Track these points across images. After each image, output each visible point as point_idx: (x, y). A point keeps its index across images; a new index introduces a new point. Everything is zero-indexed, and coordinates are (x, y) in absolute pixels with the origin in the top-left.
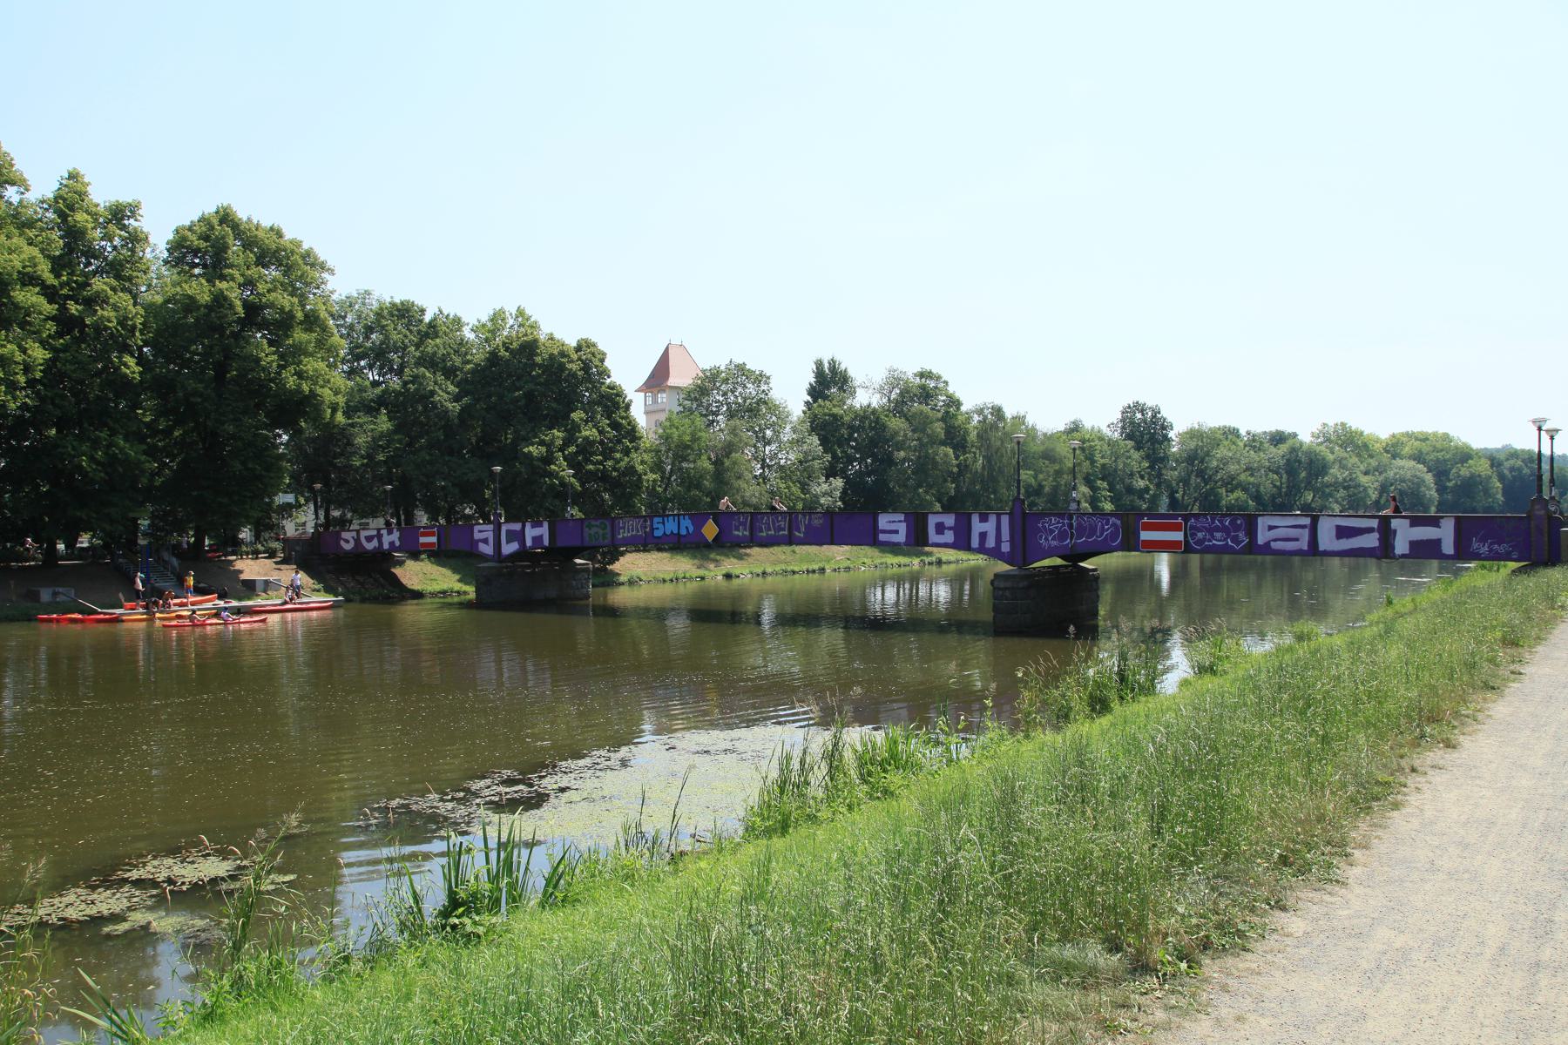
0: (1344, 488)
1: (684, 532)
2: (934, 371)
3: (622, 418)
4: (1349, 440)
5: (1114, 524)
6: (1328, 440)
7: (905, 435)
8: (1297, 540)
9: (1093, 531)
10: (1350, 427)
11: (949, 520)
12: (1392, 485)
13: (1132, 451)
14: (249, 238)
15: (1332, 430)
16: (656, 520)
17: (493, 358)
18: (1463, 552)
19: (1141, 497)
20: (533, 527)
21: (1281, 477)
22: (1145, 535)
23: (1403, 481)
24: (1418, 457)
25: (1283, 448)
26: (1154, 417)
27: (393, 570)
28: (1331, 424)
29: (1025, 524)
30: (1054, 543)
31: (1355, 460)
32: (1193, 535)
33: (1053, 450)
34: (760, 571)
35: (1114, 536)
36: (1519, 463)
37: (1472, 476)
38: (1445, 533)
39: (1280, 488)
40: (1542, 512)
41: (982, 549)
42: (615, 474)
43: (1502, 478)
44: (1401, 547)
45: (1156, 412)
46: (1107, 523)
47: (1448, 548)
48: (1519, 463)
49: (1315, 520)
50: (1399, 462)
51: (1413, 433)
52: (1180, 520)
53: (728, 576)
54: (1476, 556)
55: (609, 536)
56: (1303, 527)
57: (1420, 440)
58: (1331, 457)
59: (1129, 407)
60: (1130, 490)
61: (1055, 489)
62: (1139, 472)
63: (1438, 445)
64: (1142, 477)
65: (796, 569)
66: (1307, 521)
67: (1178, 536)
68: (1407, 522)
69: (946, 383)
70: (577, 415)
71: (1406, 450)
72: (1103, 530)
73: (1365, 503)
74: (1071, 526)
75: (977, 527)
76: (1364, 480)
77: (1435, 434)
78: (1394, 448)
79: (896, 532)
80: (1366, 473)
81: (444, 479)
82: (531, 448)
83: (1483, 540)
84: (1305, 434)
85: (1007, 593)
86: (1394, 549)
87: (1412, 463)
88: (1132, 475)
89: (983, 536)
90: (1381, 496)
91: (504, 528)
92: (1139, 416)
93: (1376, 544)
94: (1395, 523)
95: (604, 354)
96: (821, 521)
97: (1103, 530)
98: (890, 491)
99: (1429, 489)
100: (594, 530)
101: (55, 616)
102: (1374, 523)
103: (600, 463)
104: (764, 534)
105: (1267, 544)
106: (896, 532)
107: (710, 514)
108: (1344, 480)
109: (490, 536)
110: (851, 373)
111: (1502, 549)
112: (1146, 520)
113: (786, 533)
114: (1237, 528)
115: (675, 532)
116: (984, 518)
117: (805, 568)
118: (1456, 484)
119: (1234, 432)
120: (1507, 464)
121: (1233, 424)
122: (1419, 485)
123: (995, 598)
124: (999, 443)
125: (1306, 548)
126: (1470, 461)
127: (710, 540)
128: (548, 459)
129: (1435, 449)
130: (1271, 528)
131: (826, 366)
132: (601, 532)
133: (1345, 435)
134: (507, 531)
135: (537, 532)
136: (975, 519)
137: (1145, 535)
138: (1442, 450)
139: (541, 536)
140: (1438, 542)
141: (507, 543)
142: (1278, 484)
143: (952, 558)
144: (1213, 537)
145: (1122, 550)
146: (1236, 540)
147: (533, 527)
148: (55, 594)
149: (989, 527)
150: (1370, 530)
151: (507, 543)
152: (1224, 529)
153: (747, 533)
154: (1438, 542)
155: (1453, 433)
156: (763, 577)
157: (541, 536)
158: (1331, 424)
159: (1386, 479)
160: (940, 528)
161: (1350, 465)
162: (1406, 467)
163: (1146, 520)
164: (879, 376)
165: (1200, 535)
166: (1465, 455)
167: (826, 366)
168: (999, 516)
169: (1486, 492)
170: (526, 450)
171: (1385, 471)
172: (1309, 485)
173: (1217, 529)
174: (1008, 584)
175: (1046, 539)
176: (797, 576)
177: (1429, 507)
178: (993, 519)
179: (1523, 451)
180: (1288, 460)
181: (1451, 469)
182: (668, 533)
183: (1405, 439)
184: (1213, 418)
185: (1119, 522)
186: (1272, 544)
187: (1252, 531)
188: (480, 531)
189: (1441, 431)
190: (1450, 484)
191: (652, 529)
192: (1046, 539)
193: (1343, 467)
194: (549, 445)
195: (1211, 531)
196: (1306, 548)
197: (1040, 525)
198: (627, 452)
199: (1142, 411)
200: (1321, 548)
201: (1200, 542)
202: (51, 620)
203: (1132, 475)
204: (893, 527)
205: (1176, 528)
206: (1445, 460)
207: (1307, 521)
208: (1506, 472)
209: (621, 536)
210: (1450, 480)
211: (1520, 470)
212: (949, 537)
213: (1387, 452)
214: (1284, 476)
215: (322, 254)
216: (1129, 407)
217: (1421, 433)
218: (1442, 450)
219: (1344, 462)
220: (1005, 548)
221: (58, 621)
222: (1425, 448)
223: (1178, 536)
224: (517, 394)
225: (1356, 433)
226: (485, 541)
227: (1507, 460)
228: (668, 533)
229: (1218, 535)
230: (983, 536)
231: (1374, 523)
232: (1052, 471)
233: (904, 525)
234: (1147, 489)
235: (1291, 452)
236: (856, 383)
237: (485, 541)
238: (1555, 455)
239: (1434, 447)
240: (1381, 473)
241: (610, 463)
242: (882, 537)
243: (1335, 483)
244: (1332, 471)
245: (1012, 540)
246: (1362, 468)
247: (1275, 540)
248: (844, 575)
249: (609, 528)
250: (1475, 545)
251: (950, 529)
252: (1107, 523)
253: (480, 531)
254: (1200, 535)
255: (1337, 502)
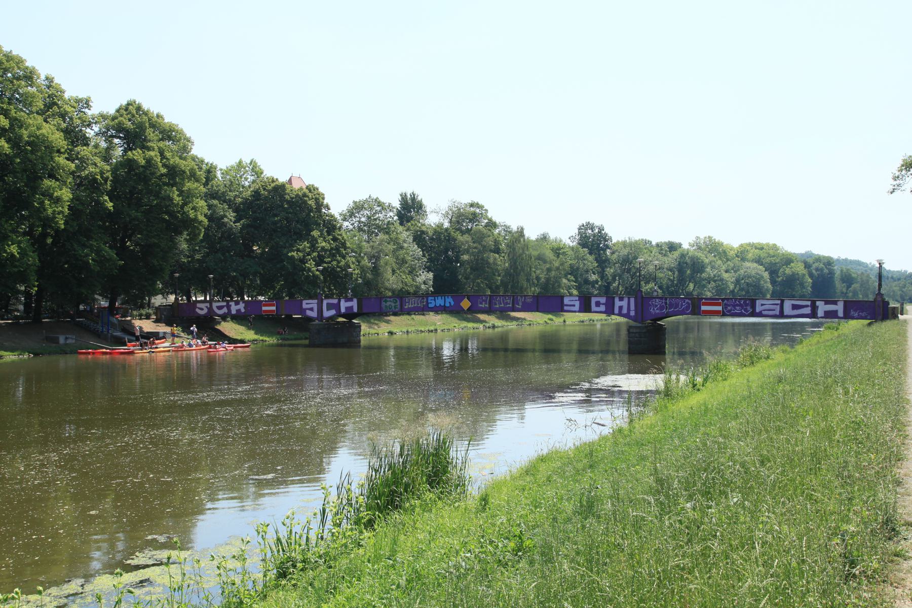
0: (715, 281)
1: (447, 305)
2: (480, 203)
3: (338, 235)
4: (714, 248)
5: (688, 303)
6: (699, 248)
7: (469, 246)
8: (774, 310)
9: (677, 306)
10: (715, 239)
11: (603, 300)
12: (742, 279)
13: (588, 255)
14: (155, 123)
15: (702, 242)
16: (430, 298)
17: (256, 193)
18: (847, 316)
19: (593, 287)
20: (346, 301)
21: (674, 274)
22: (704, 308)
23: (749, 277)
24: (759, 261)
25: (676, 254)
26: (599, 232)
27: (216, 327)
28: (702, 237)
29: (643, 301)
30: (658, 311)
31: (719, 262)
32: (726, 308)
33: (544, 254)
34: (405, 330)
35: (687, 308)
36: (822, 265)
37: (793, 274)
38: (840, 308)
39: (672, 281)
40: (880, 299)
41: (620, 314)
42: (339, 269)
43: (811, 275)
44: (820, 313)
45: (601, 229)
46: (684, 302)
47: (841, 314)
48: (822, 265)
49: (782, 301)
50: (747, 264)
51: (753, 244)
52: (720, 301)
53: (391, 333)
54: (853, 318)
55: (399, 307)
56: (567, 305)
57: (759, 249)
58: (707, 261)
59: (583, 226)
60: (587, 281)
61: (548, 280)
62: (592, 270)
63: (771, 252)
64: (594, 274)
65: (423, 330)
66: (779, 302)
67: (720, 308)
68: (823, 302)
69: (486, 210)
70: (315, 233)
71: (750, 256)
72: (682, 305)
73: (726, 291)
74: (666, 303)
75: (618, 303)
76: (726, 276)
77: (768, 245)
78: (742, 254)
79: (574, 306)
80: (726, 271)
81: (234, 271)
82: (293, 253)
83: (855, 311)
84: (686, 242)
85: (637, 335)
86: (817, 314)
87: (755, 265)
88: (587, 271)
89: (621, 308)
90: (735, 288)
91: (325, 302)
92: (590, 231)
93: (810, 312)
94: (818, 303)
95: (323, 195)
96: (531, 300)
97: (682, 305)
98: (458, 281)
99: (766, 282)
100: (388, 303)
101: (90, 350)
102: (809, 303)
103: (329, 262)
104: (498, 306)
105: (761, 312)
106: (574, 306)
107: (465, 296)
108: (715, 276)
109: (315, 307)
110: (424, 202)
111: (863, 314)
112: (704, 301)
113: (511, 305)
114: (747, 305)
115: (443, 304)
116: (621, 299)
117: (427, 329)
118: (783, 280)
119: (647, 242)
120: (814, 266)
121: (648, 238)
122: (759, 280)
123: (629, 337)
124: (521, 251)
125: (778, 314)
126: (792, 264)
127: (466, 309)
128: (303, 261)
129: (769, 256)
130: (762, 305)
131: (409, 196)
132: (393, 305)
133: (711, 245)
134: (327, 304)
135: (349, 304)
136: (617, 300)
137: (704, 308)
138: (773, 256)
139: (352, 307)
140: (836, 312)
141: (327, 310)
142: (672, 278)
143: (500, 324)
144: (736, 309)
145: (692, 315)
146: (746, 310)
147: (346, 301)
148: (66, 338)
149: (624, 303)
150: (807, 306)
151: (327, 310)
152: (740, 305)
153: (487, 306)
154: (836, 312)
155: (779, 244)
156: (407, 334)
157: (352, 307)
158: (702, 237)
159: (740, 275)
160: (598, 304)
161: (717, 266)
162: (752, 268)
163: (704, 301)
164: (444, 206)
165: (729, 308)
166: (788, 260)
167: (409, 196)
168: (629, 298)
169: (802, 285)
170: (290, 254)
171: (738, 270)
172: (692, 278)
173: (737, 305)
174: (638, 331)
175: (654, 309)
176: (423, 334)
177: (766, 295)
178: (626, 300)
179: (824, 257)
180: (679, 262)
181: (779, 269)
182: (438, 305)
183: (749, 248)
184: (636, 235)
185: (690, 302)
186: (763, 312)
187: (753, 306)
188: (307, 304)
189: (771, 242)
190: (780, 279)
191: (428, 303)
192: (654, 309)
193: (713, 267)
194: (303, 251)
195: (734, 306)
196: (778, 314)
197: (650, 303)
198: (344, 257)
199: (592, 229)
200: (785, 314)
201: (729, 311)
202: (89, 353)
203: (587, 271)
204: (572, 303)
205: (718, 304)
206: (776, 263)
207: (779, 302)
208: (814, 272)
209: (407, 307)
210: (779, 277)
211: (822, 270)
212: (603, 308)
213: (738, 256)
214: (676, 273)
215: (193, 139)
216: (583, 226)
217: (759, 244)
218: (773, 256)
219: (713, 263)
220: (632, 313)
221: (93, 353)
222: (762, 254)
223: (720, 308)
224: (276, 219)
225: (719, 243)
226: (312, 309)
227: (814, 263)
228: (438, 305)
229: (738, 308)
230: (621, 308)
231: (809, 303)
232: (545, 269)
233: (578, 302)
234: (597, 282)
235: (681, 257)
236: (428, 210)
237: (312, 309)
238: (884, 273)
239: (769, 254)
240: (735, 272)
241: (335, 263)
242: (566, 308)
243: (709, 278)
244: (708, 270)
245: (636, 310)
246: (724, 268)
247: (764, 310)
248: (491, 331)
249: (398, 303)
250: (852, 313)
251: (603, 304)
252: (684, 302)
253: (307, 304)
254: (729, 308)
255: (709, 291)
